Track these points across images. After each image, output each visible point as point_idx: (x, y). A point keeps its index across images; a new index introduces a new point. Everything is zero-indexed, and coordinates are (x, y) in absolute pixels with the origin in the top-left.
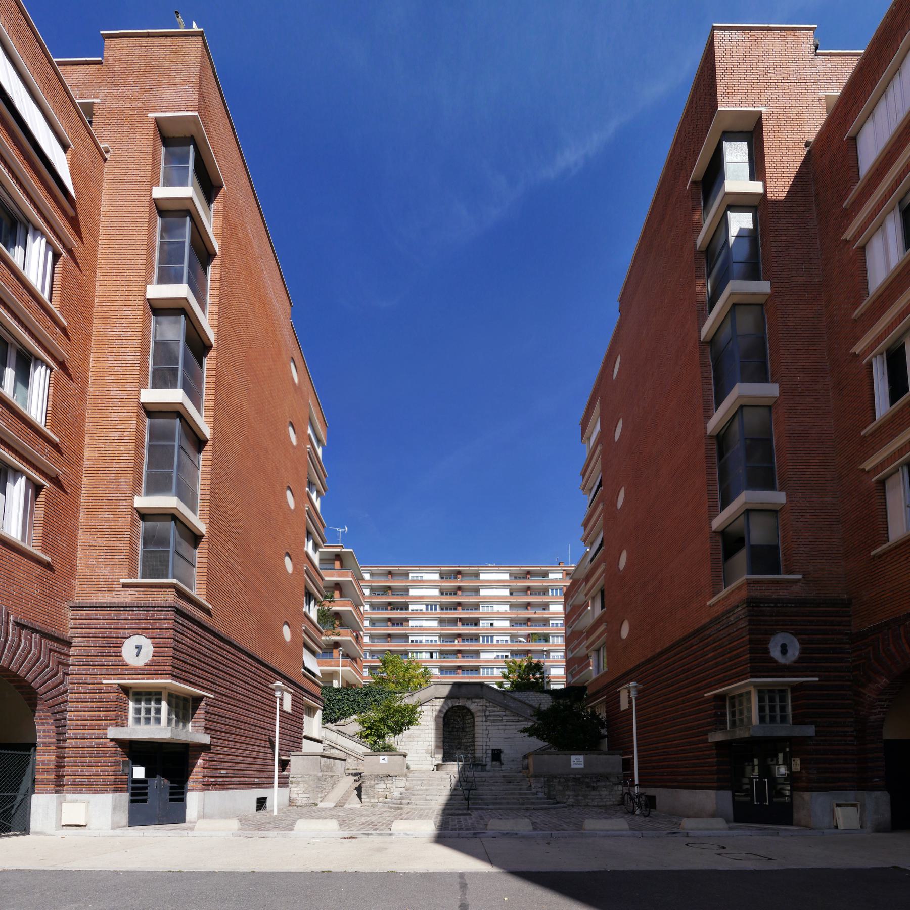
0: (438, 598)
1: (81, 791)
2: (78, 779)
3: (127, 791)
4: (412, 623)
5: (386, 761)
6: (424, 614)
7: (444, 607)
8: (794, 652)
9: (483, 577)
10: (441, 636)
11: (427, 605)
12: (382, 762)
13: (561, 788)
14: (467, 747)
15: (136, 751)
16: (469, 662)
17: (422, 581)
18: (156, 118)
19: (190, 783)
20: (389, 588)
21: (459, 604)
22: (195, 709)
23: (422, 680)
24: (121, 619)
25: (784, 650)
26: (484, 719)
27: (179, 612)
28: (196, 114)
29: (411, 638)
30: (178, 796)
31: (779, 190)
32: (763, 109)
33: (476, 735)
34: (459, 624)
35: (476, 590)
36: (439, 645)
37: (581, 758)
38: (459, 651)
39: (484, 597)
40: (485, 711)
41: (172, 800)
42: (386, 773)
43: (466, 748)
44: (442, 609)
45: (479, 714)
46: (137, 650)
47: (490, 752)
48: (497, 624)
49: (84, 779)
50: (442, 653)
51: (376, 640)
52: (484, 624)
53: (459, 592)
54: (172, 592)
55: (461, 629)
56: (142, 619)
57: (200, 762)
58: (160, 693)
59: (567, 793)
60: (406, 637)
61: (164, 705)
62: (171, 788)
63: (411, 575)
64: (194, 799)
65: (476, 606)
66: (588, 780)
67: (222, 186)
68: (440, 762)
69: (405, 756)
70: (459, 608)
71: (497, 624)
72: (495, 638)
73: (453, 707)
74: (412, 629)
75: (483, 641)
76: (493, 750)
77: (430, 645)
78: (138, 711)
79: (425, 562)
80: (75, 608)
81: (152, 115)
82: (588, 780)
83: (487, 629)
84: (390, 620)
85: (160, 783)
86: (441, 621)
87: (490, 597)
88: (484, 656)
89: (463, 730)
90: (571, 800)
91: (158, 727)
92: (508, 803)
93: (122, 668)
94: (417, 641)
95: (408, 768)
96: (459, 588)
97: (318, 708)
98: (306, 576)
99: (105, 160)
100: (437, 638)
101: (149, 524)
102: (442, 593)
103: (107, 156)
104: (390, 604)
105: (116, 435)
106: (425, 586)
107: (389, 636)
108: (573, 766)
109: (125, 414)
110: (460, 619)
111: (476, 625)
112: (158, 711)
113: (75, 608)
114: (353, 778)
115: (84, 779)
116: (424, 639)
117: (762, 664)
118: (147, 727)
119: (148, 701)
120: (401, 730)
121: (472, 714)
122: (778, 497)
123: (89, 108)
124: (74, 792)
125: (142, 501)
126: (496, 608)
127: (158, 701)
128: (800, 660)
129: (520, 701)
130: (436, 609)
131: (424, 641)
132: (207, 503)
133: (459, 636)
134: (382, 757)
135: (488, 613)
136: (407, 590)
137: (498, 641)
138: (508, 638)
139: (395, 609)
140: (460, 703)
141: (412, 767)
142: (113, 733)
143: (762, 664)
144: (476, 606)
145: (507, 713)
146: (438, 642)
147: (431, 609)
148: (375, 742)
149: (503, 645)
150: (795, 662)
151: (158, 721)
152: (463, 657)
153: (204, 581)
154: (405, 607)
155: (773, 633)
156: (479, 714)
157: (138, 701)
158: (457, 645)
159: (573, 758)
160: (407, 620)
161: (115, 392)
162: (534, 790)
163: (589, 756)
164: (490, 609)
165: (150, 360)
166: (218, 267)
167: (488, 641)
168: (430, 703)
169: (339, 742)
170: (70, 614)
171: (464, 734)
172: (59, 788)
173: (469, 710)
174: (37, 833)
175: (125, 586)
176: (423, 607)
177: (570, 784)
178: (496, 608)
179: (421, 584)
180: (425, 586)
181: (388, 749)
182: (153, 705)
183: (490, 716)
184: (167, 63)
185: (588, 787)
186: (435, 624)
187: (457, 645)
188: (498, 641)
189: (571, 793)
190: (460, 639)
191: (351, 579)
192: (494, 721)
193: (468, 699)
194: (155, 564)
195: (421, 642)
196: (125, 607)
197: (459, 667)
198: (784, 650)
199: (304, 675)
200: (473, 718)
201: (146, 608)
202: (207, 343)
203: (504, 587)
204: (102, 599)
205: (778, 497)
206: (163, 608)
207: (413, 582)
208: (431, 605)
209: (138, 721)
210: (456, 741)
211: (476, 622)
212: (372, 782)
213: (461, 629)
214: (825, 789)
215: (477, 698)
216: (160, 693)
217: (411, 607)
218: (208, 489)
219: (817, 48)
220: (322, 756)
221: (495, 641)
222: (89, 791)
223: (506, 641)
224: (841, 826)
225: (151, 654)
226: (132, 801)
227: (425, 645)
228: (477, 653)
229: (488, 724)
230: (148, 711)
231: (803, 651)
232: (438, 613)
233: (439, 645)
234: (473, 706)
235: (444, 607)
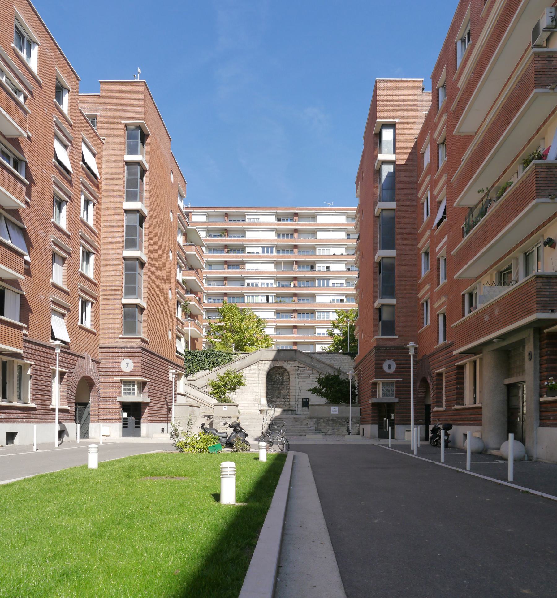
0: (274, 240)
1: (106, 422)
2: (105, 418)
3: (120, 422)
4: (248, 266)
5: (226, 409)
6: (260, 257)
7: (280, 249)
8: (394, 368)
9: (319, 219)
10: (277, 279)
11: (263, 248)
12: (224, 409)
13: (324, 424)
14: (284, 396)
15: (126, 406)
16: (304, 305)
17: (257, 224)
18: (125, 123)
19: (142, 420)
20: (226, 230)
21: (296, 247)
22: (144, 387)
23: (256, 329)
24: (119, 352)
25: (389, 367)
26: (297, 376)
27: (143, 349)
28: (143, 121)
29: (247, 281)
30: (138, 424)
31: (402, 160)
32: (397, 120)
33: (290, 388)
34: (295, 267)
35: (313, 233)
36: (275, 289)
37: (337, 408)
38: (295, 295)
39: (320, 240)
40: (297, 370)
41: (136, 427)
42: (226, 415)
43: (284, 396)
44: (278, 251)
45: (293, 372)
46: (127, 365)
47: (301, 400)
48: (333, 267)
49: (108, 418)
50: (277, 295)
51: (213, 283)
52: (320, 267)
53: (296, 235)
54: (140, 340)
55: (298, 272)
56: (129, 352)
57: (146, 410)
58: (134, 382)
59: (328, 427)
60: (243, 279)
61: (136, 387)
62: (136, 422)
63: (247, 217)
64: (144, 426)
65: (313, 249)
66: (340, 421)
67: (149, 135)
68: (265, 408)
69: (237, 406)
70: (296, 251)
71: (333, 267)
72: (331, 282)
73: (274, 367)
74: (248, 273)
75: (319, 284)
76: (303, 399)
77: (266, 289)
78: (125, 389)
79: (262, 206)
80: (101, 348)
81: (123, 122)
82: (340, 421)
83: (323, 273)
84: (226, 262)
85: (132, 420)
86: (277, 264)
87: (327, 240)
88: (319, 299)
89: (282, 383)
90: (330, 432)
91: (133, 396)
92: (292, 432)
93: (120, 372)
94: (253, 284)
95: (239, 413)
96: (296, 231)
97: (183, 374)
98: (177, 295)
99: (103, 144)
100: (273, 281)
101: (126, 309)
102: (279, 235)
103: (104, 141)
104: (226, 246)
105: (113, 272)
106: (261, 229)
107: (226, 278)
108: (332, 413)
109: (117, 263)
110: (296, 263)
111: (312, 267)
112: (133, 390)
113: (101, 348)
114: (206, 418)
115: (108, 418)
116: (260, 282)
117: (380, 373)
118: (129, 396)
119: (129, 385)
120: (235, 389)
121: (288, 372)
122: (393, 301)
123: (94, 119)
124: (103, 422)
125: (125, 301)
126: (333, 251)
127: (134, 385)
128: (395, 371)
129: (323, 363)
130: (272, 252)
131: (260, 285)
132: (146, 292)
133: (295, 279)
134: (224, 407)
135: (325, 256)
136: (243, 232)
137: (334, 284)
138: (343, 282)
139: (233, 250)
140: (280, 364)
141: (242, 411)
142: (119, 399)
143: (380, 373)
144: (313, 249)
145: (314, 372)
146: (275, 285)
147: (268, 252)
148: (220, 397)
149: (338, 289)
150: (394, 372)
151: (134, 393)
152: (299, 300)
153: (146, 329)
154: (241, 249)
155: (385, 360)
156: (293, 372)
157: (125, 385)
158: (293, 288)
159: (332, 408)
160: (243, 263)
161: (112, 253)
162: (309, 426)
163: (341, 407)
164: (326, 252)
165: (124, 235)
166: (148, 177)
167: (323, 285)
168: (257, 364)
169: (192, 394)
170: (99, 350)
171: (283, 386)
172: (98, 421)
173: (286, 370)
174: (92, 438)
175: (120, 338)
176: (260, 250)
177: (330, 422)
178: (333, 251)
179: (257, 226)
180: (261, 229)
181: (227, 402)
182: (131, 387)
183: (301, 374)
184: (129, 96)
185: (340, 424)
186: (271, 267)
187: (293, 288)
188: (334, 284)
189: (330, 428)
190: (296, 282)
191: (195, 253)
192: (304, 378)
193: (285, 361)
194: (130, 326)
195: (257, 286)
196: (122, 348)
197: (295, 311)
198: (389, 367)
199: (177, 356)
200: (289, 375)
201: (130, 348)
202: (144, 215)
203: (341, 230)
204: (111, 344)
205: (393, 301)
206: (137, 348)
207: (249, 224)
208: (268, 248)
209: (125, 393)
210: (277, 392)
211: (312, 266)
212: (219, 421)
213: (298, 272)
214: (403, 424)
215: (291, 361)
216: (134, 382)
217: (248, 250)
218: (146, 287)
219: (423, 89)
220: (190, 406)
221: (331, 285)
222: (110, 422)
223: (342, 284)
224: (406, 439)
225: (133, 367)
226: (123, 427)
227: (262, 289)
228: (313, 296)
229: (299, 380)
230: (129, 389)
231: (397, 368)
232: (275, 256)
233: (275, 289)
234: (289, 366)
235: (280, 249)
